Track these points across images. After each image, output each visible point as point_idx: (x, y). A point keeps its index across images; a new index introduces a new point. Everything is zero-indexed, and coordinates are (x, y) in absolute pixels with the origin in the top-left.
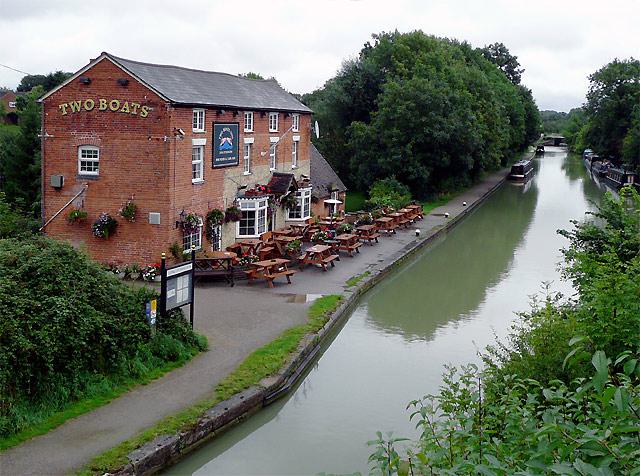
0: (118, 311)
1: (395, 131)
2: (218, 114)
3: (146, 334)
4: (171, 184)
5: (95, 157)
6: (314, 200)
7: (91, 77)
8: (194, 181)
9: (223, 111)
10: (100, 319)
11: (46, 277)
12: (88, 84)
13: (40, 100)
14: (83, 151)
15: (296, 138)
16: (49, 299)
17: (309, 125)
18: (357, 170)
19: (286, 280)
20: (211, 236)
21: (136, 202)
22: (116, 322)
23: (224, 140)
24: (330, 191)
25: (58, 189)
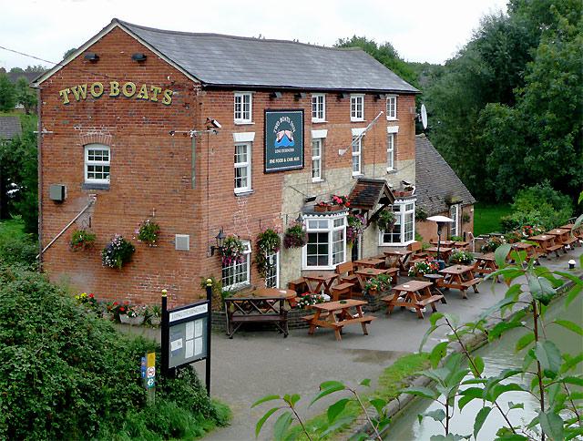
0: (102, 368)
1: (549, 115)
2: (272, 97)
3: (140, 401)
4: (203, 195)
5: (106, 159)
6: (421, 217)
7: (98, 53)
8: (237, 190)
9: (278, 94)
10: (74, 377)
11: (6, 319)
12: (96, 60)
13: (36, 85)
14: (90, 152)
15: (393, 129)
16: (7, 349)
17: (413, 109)
18: (496, 172)
19: (360, 329)
20: (261, 265)
21: (157, 221)
22: (98, 383)
23: (281, 134)
24: (449, 204)
25: (59, 203)
